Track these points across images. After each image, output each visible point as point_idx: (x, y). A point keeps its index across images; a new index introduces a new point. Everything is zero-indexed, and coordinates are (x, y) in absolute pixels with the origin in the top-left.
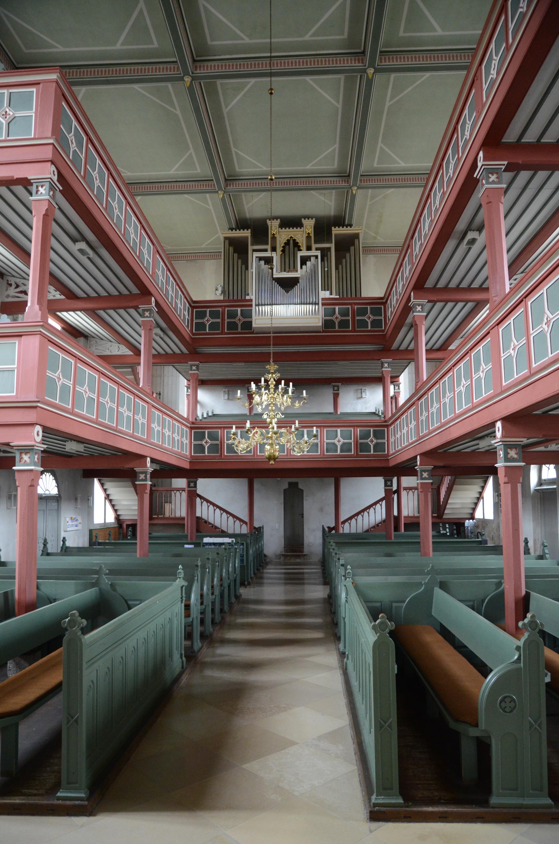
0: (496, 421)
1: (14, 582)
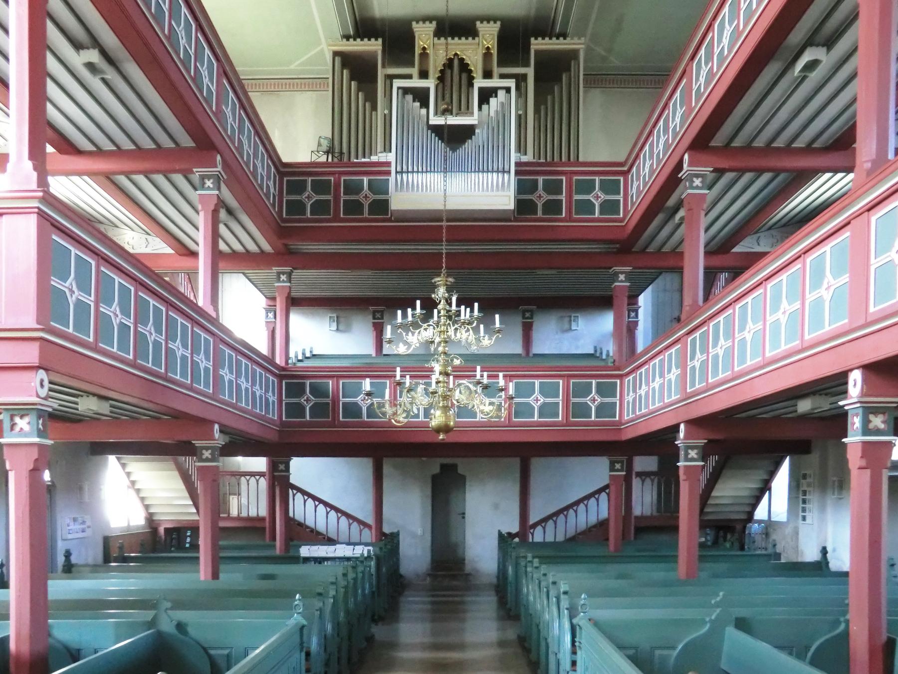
1: (9, 625)
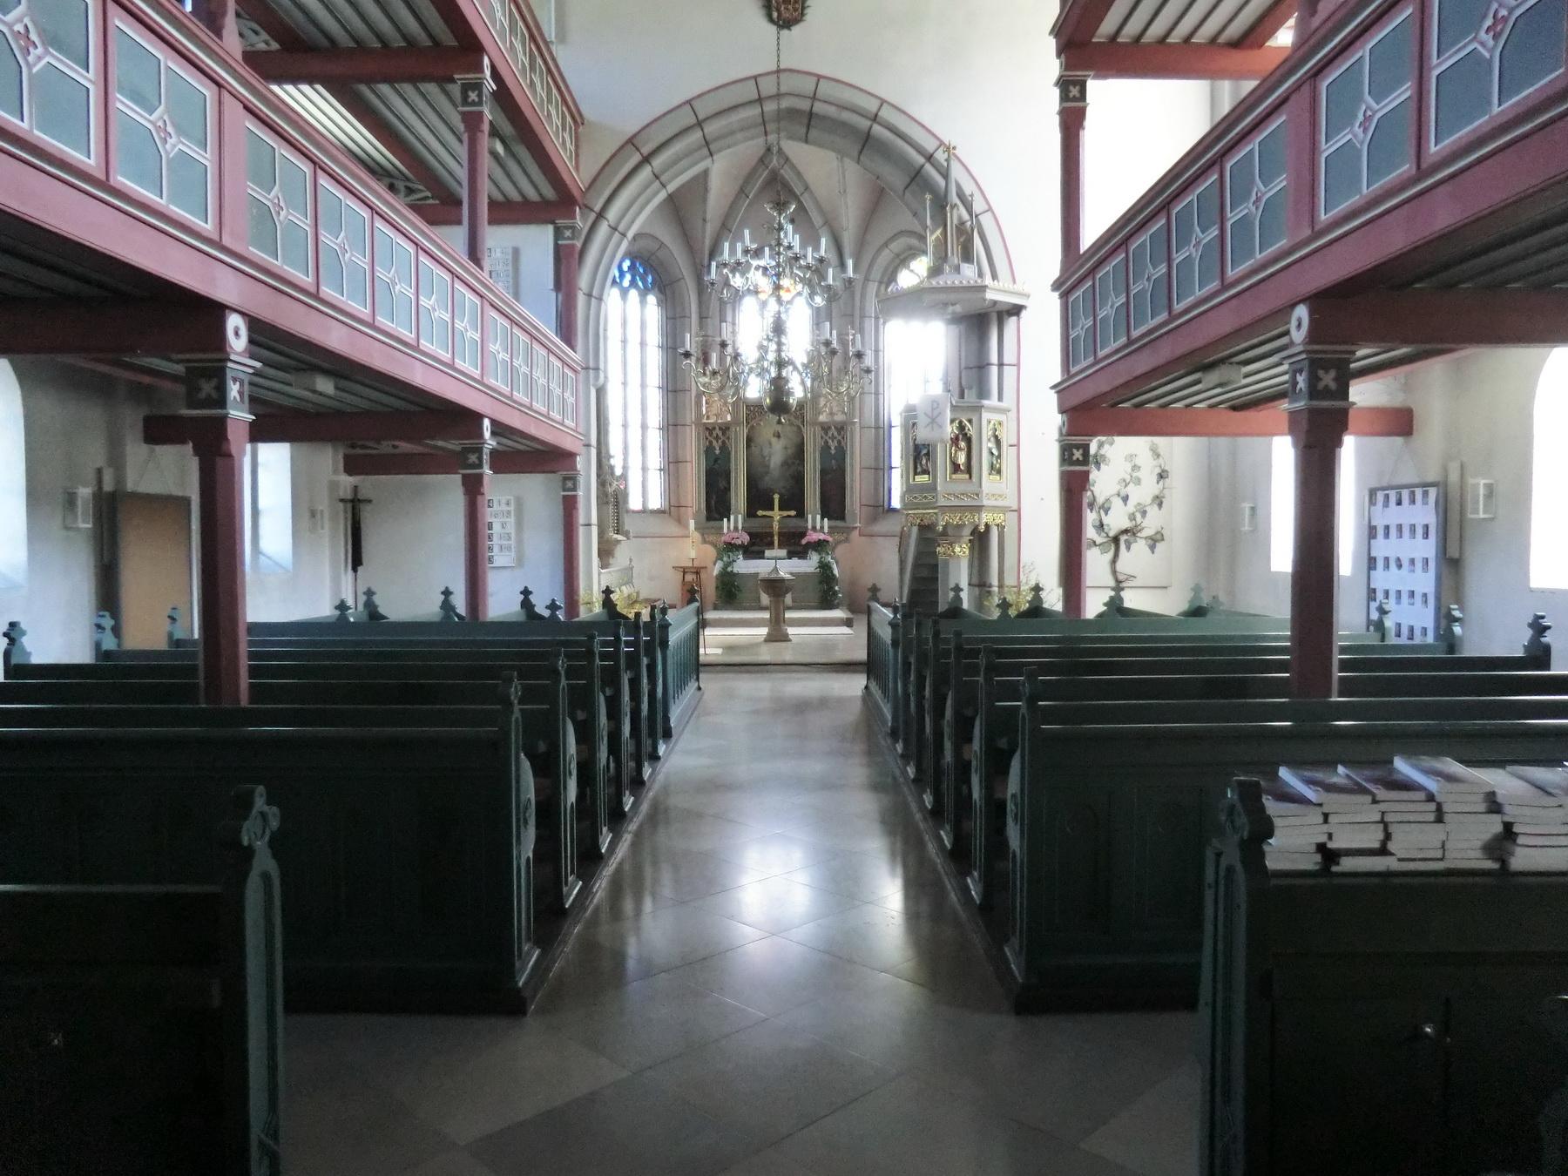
0: (1293, 306)
